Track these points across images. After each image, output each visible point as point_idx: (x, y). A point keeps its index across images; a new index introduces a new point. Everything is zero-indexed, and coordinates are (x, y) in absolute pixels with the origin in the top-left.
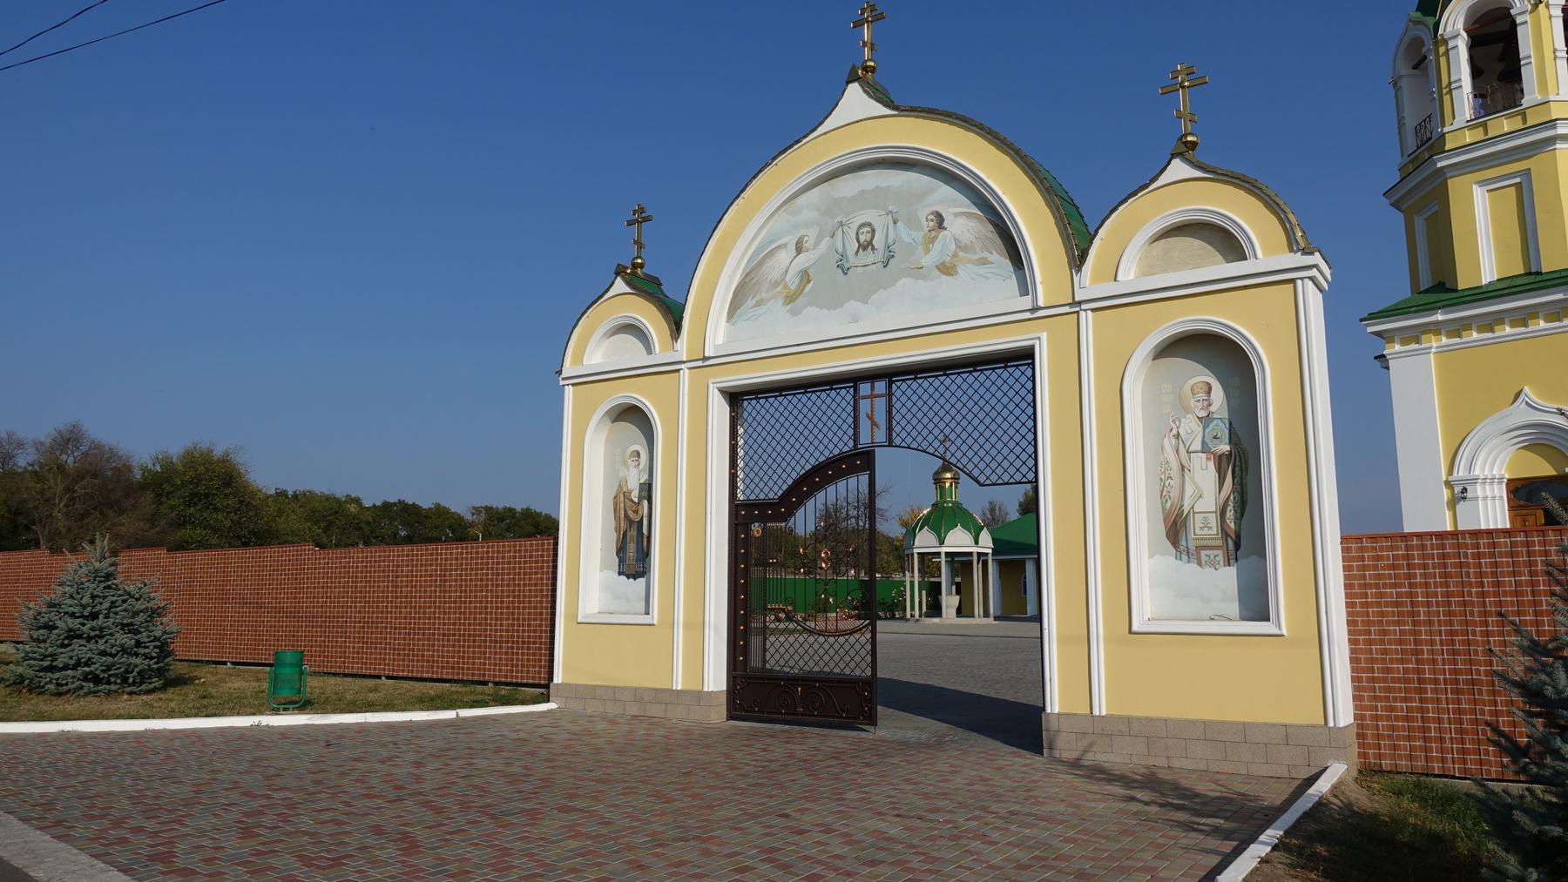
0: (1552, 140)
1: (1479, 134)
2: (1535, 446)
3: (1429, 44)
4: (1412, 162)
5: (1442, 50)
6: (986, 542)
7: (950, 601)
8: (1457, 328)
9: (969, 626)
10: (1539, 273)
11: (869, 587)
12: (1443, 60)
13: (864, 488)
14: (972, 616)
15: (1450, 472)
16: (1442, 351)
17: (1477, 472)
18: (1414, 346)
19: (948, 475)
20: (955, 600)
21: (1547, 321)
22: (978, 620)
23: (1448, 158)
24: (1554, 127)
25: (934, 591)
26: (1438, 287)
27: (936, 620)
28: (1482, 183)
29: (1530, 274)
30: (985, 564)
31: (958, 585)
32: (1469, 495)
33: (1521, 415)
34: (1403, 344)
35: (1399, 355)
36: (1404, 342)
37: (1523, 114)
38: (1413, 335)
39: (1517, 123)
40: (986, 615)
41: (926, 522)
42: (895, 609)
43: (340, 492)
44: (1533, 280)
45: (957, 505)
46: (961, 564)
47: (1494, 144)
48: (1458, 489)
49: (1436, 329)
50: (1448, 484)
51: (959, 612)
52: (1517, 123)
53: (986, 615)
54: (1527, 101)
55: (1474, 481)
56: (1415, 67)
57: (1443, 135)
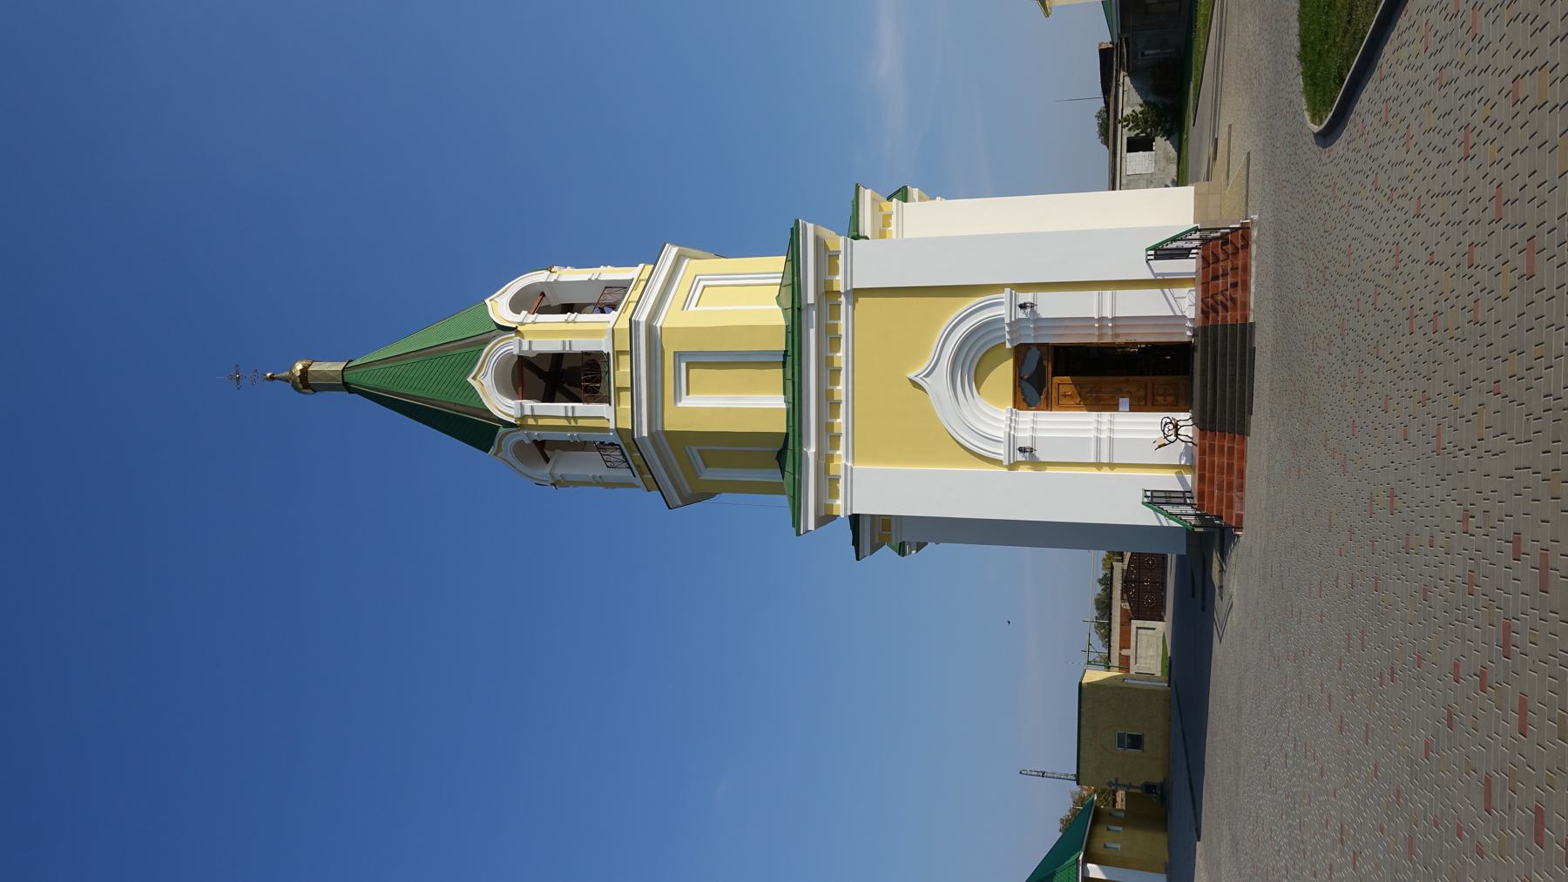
0: (651, 329)
2: (978, 378)
3: (521, 435)
4: (642, 474)
5: (531, 422)
8: (829, 438)
10: (785, 354)
12: (541, 422)
13: (645, 276)
15: (998, 462)
16: (852, 454)
17: (1001, 434)
23: (640, 425)
24: (638, 323)
26: (780, 453)
28: (677, 397)
29: (784, 363)
32: (1028, 444)
33: (939, 384)
34: (837, 273)
35: (849, 273)
36: (834, 270)
37: (620, 353)
38: (829, 485)
39: (625, 359)
44: (791, 360)
48: (1020, 457)
49: (824, 459)
50: (1013, 466)
52: (625, 359)
55: (1011, 439)
56: (547, 460)
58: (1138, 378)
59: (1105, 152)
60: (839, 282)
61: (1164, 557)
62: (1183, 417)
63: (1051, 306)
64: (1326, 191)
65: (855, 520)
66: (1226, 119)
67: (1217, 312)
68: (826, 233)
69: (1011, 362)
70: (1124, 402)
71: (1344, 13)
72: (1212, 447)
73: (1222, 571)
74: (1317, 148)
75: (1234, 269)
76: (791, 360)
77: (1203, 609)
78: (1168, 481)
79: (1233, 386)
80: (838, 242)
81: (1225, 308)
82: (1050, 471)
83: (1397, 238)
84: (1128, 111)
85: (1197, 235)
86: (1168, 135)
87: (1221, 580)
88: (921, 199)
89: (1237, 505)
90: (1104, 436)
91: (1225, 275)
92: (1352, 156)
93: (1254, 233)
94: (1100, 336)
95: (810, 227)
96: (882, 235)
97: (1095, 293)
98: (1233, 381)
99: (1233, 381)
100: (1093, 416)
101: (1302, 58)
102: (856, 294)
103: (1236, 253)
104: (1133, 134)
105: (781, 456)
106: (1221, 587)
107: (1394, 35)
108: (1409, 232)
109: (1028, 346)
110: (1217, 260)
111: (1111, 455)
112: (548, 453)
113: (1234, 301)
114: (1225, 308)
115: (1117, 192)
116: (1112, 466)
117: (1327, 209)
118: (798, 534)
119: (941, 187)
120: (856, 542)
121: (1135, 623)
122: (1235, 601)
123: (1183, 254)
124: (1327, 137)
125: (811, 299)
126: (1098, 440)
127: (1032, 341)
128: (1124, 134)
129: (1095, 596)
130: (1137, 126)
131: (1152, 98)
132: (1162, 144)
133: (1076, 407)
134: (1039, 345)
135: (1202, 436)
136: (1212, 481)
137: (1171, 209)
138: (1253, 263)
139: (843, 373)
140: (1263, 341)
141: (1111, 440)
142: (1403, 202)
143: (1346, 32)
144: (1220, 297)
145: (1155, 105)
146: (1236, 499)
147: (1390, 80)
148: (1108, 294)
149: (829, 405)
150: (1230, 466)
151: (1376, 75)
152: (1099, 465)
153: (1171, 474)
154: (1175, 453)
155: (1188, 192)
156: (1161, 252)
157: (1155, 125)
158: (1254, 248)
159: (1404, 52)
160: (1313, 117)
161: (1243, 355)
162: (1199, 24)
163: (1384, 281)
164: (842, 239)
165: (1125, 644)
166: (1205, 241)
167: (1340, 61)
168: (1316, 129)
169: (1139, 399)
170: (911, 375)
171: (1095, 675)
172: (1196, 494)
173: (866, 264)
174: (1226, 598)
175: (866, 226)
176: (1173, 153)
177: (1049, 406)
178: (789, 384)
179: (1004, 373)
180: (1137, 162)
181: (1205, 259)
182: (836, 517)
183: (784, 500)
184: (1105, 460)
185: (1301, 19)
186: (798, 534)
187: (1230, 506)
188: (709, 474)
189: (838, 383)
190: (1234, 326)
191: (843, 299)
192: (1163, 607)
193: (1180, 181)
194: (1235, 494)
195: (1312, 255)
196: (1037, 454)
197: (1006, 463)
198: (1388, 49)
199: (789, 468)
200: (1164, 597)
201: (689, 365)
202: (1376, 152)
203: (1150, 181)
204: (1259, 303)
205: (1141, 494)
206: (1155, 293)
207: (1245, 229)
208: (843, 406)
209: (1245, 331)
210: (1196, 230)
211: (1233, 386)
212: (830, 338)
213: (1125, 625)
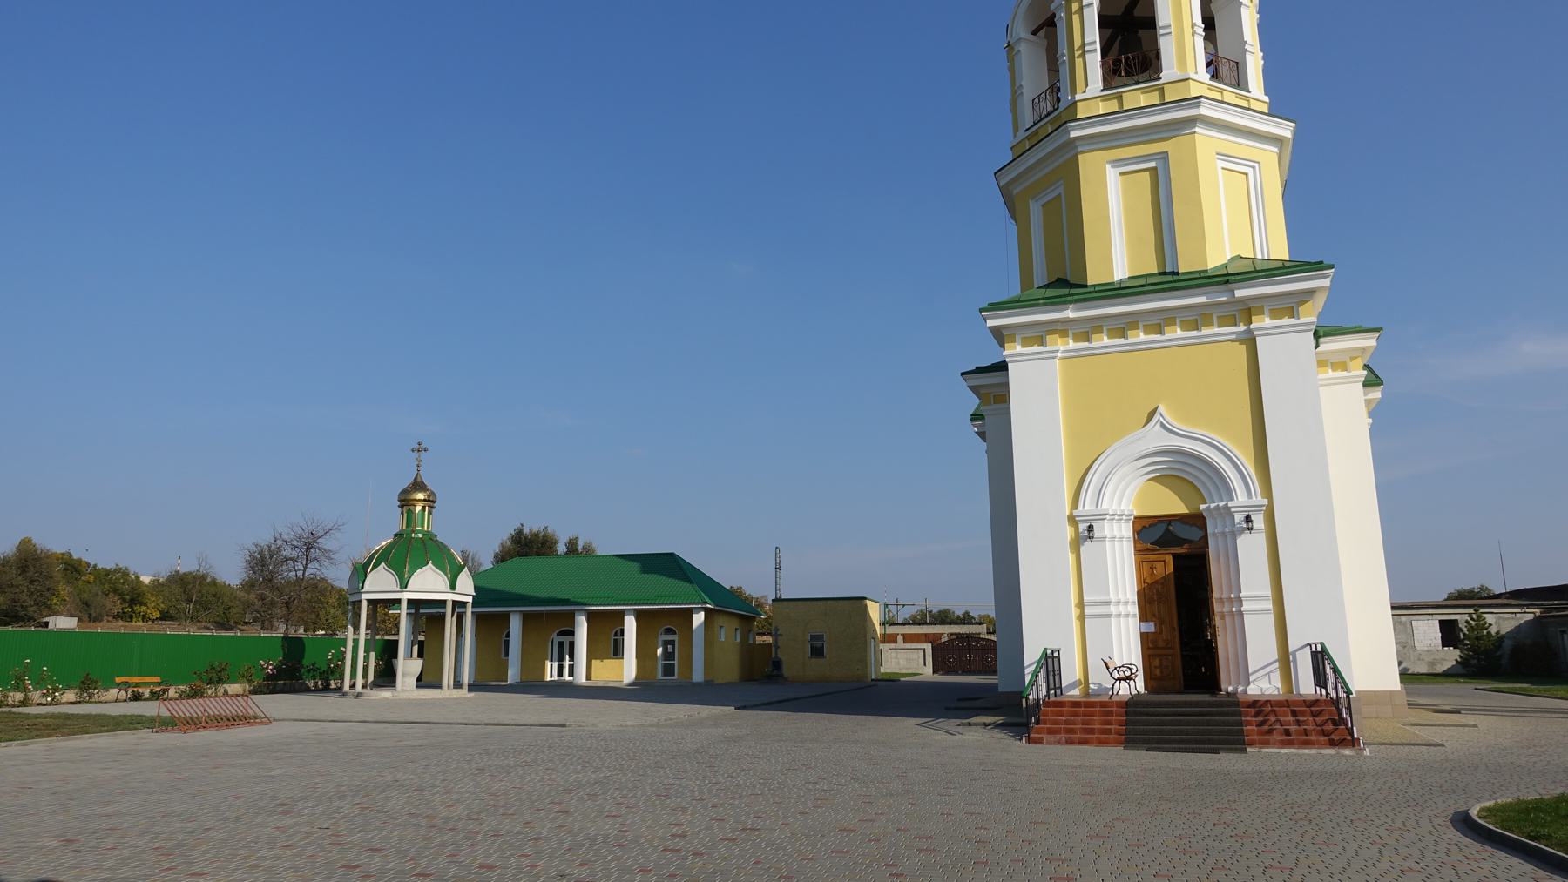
0: (1192, 121)
1: (1113, 106)
6: (466, 587)
7: (408, 667)
8: (1085, 330)
9: (433, 702)
11: (293, 648)
12: (1076, 18)
14: (439, 686)
16: (1070, 357)
17: (1105, 506)
18: (1286, 321)
19: (421, 496)
20: (416, 665)
21: (1146, 333)
22: (447, 693)
24: (1197, 106)
25: (388, 652)
26: (1063, 280)
27: (386, 694)
28: (1116, 163)
29: (1165, 273)
30: (460, 618)
31: (421, 644)
32: (1097, 534)
34: (1272, 318)
36: (1275, 314)
37: (1162, 91)
38: (1037, 335)
39: (1154, 98)
40: (458, 685)
41: (384, 557)
42: (327, 680)
43: (1467, 588)
44: (1169, 280)
45: (430, 538)
46: (428, 616)
47: (1133, 117)
48: (1083, 527)
49: (1062, 328)
50: (1072, 520)
51: (421, 682)
52: (1154, 98)
53: (458, 685)
54: (1167, 74)
55: (1102, 517)
56: (1034, 33)
57: (1075, 103)
60: (1262, 322)
61: (995, 672)
62: (1139, 685)
63: (1251, 549)
65: (1002, 367)
67: (1257, 715)
68: (1319, 302)
69: (1184, 510)
70: (1150, 627)
72: (1111, 713)
73: (986, 725)
74: (1450, 813)
75: (1306, 732)
76: (1169, 280)
77: (948, 709)
78: (1071, 672)
79: (1175, 732)
80: (1309, 316)
82: (1071, 558)
84: (1489, 619)
85: (1342, 694)
86: (1463, 663)
88: (1368, 402)
89: (1051, 738)
90: (1113, 609)
91: (1298, 723)
92: (1442, 847)
93: (1348, 752)
94: (1221, 600)
95: (1327, 282)
96: (1322, 363)
98: (1181, 733)
99: (1181, 733)
100: (1132, 596)
102: (1250, 341)
103: (1324, 733)
104: (1462, 625)
105: (1062, 282)
109: (1204, 527)
110: (1314, 715)
111: (1093, 616)
112: (1042, 33)
113: (1270, 732)
115: (1390, 612)
116: (1082, 617)
118: (981, 310)
119: (1383, 424)
121: (928, 647)
122: (958, 737)
123: (1320, 680)
125: (1239, 293)
126: (1108, 603)
127: (1210, 530)
128: (1461, 617)
130: (1471, 629)
131: (1508, 644)
132: (1452, 656)
134: (1205, 538)
135: (1119, 704)
136: (1055, 722)
137: (1371, 664)
138: (1313, 751)
140: (1227, 761)
141: (1109, 615)
148: (1269, 605)
149: (1122, 326)
150: (1092, 731)
152: (1081, 604)
153: (1078, 675)
154: (1100, 679)
156: (1320, 658)
157: (1474, 649)
160: (1489, 810)
161: (1211, 742)
165: (908, 638)
166: (1336, 702)
170: (1162, 409)
171: (875, 612)
172: (1059, 699)
175: (1331, 345)
178: (1142, 282)
179: (1173, 505)
180: (1428, 631)
181: (1315, 702)
183: (1015, 291)
184: (1087, 611)
186: (981, 310)
187: (1050, 732)
188: (1035, 211)
190: (1241, 732)
191: (1243, 328)
193: (1405, 676)
194: (1063, 737)
195: (1325, 807)
197: (1075, 513)
200: (955, 672)
201: (1153, 171)
203: (1405, 645)
204: (1267, 757)
206: (1274, 654)
207: (1353, 743)
209: (1235, 742)
210: (1348, 693)
211: (1175, 732)
213: (926, 638)
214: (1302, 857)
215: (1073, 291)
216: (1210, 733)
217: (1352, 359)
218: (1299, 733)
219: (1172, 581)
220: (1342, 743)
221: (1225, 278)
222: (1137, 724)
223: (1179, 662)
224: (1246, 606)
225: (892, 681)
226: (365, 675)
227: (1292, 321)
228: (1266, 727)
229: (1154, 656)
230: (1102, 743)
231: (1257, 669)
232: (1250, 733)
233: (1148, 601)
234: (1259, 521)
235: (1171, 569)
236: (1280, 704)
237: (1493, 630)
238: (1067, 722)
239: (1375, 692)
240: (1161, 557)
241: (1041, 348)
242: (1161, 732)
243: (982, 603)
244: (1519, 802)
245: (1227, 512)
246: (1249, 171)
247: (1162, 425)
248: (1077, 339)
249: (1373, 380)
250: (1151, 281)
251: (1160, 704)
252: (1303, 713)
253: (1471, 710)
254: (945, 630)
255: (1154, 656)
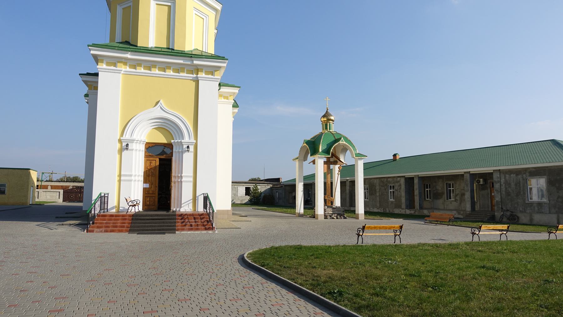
2: (159, 129)
8: (135, 64)
16: (127, 74)
17: (135, 137)
18: (210, 76)
26: (127, 41)
29: (169, 49)
32: (130, 147)
33: (157, 112)
34: (206, 74)
35: (105, 71)
36: (207, 73)
38: (114, 62)
48: (124, 144)
49: (125, 61)
50: (120, 141)
55: (132, 141)
58: (157, 191)
59: (247, 180)
60: (201, 75)
61: (81, 201)
62: (140, 208)
63: (188, 158)
64: (220, 261)
65: (96, 75)
66: (253, 219)
67: (181, 219)
68: (222, 71)
69: (166, 142)
70: (147, 186)
71: (288, 265)
72: (125, 219)
73: (70, 225)
74: (238, 256)
75: (198, 225)
76: (170, 51)
77: (57, 217)
78: (112, 203)
79: (150, 226)
80: (218, 75)
81: (182, 223)
82: (118, 156)
83: (193, 299)
84: (259, 187)
85: (211, 211)
86: (250, 200)
87: (66, 225)
88: (233, 113)
89: (98, 230)
90: (133, 178)
91: (196, 222)
92: (233, 272)
93: (210, 232)
94: (175, 177)
95: (225, 65)
96: (220, 96)
97: (192, 175)
98: (153, 226)
99: (153, 226)
100: (141, 173)
101: (272, 248)
102: (197, 81)
103: (204, 225)
104: (251, 189)
105: (127, 43)
106: (63, 225)
107: (279, 288)
108: (194, 305)
109: (172, 149)
110: (201, 219)
111: (125, 180)
113: (185, 225)
114: (182, 223)
115: (231, 183)
116: (120, 181)
117: (213, 262)
118: (88, 46)
119: (238, 123)
120: (88, 74)
121: (62, 191)
122: (55, 230)
123: (205, 207)
124: (242, 261)
125: (195, 62)
126: (131, 176)
127: (174, 150)
128: (251, 186)
129: (79, 176)
130: (254, 190)
131: (263, 195)
132: (248, 198)
133: (146, 167)
134: (172, 153)
135: (130, 216)
136: (101, 223)
137: (222, 202)
138: (199, 232)
139: (163, 73)
140: (168, 238)
141: (131, 181)
142: (208, 300)
143: (281, 266)
144: (187, 220)
145: (260, 196)
146: (101, 229)
147: (261, 288)
148: (191, 179)
149: (150, 66)
150: (116, 227)
151: (264, 281)
152: (120, 176)
153: (116, 204)
154: (124, 205)
155: (229, 207)
156: (206, 198)
157: (254, 196)
158: (205, 232)
159: (272, 294)
160: (250, 254)
161: (163, 230)
162: (285, 210)
163: (174, 294)
164: (220, 77)
165: (52, 187)
166: (208, 214)
167: (267, 265)
168: (245, 256)
169: (148, 191)
170: (161, 101)
171: (34, 175)
172: (105, 214)
173: (209, 86)
174: (56, 227)
175: (224, 89)
176: (244, 202)
177: (146, 156)
178: (160, 50)
179: (161, 139)
180: (242, 190)
181: (202, 214)
182: (98, 64)
183: (107, 41)
184: (122, 178)
185: (286, 246)
186: (88, 46)
187: (98, 227)
188: (119, 10)
189: (159, 70)
190: (175, 226)
191: (195, 76)
192: (70, 201)
193: (234, 205)
194: (103, 229)
195: (196, 256)
196: (126, 151)
197: (122, 138)
198: (273, 285)
199: (121, 45)
200: (74, 201)
201: (169, 7)
202: (233, 283)
203: (234, 194)
204: (183, 235)
205: (107, 192)
206: (191, 197)
207: (212, 228)
208: (149, 72)
209: (172, 230)
210: (213, 211)
211: (150, 226)
212: (179, 69)
213: (62, 187)
214: (180, 282)
215: (131, 47)
216: (164, 226)
217: (230, 96)
218: (195, 226)
219: (158, 169)
220: (209, 229)
221: (190, 56)
222: (136, 224)
223: (157, 200)
224: (183, 179)
225: (40, 205)
226: (328, 202)
227: (212, 77)
228: (184, 224)
229: (147, 197)
230: (121, 231)
231: (184, 202)
232: (178, 226)
233: (148, 176)
234: (192, 148)
235: (158, 164)
236: (190, 215)
237: (259, 191)
238: (106, 223)
239: (223, 210)
240: (155, 159)
241: (114, 68)
242: (145, 226)
243: (82, 175)
244: (260, 250)
245: (181, 144)
246: (205, 18)
247: (161, 108)
248: (131, 67)
249: (235, 105)
250: (163, 50)
251: (146, 215)
252: (198, 218)
253: (250, 216)
254: (71, 185)
255: (147, 197)
